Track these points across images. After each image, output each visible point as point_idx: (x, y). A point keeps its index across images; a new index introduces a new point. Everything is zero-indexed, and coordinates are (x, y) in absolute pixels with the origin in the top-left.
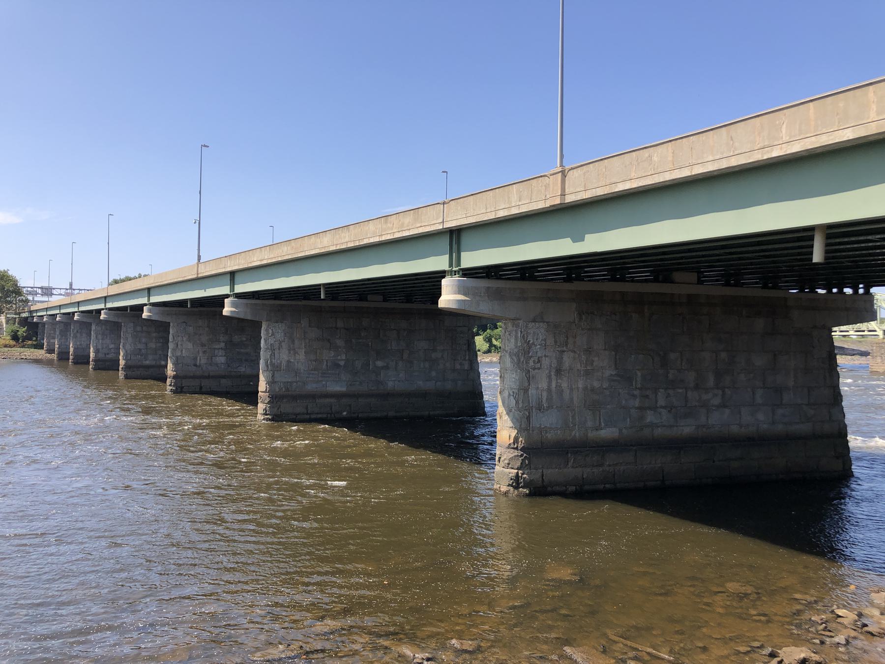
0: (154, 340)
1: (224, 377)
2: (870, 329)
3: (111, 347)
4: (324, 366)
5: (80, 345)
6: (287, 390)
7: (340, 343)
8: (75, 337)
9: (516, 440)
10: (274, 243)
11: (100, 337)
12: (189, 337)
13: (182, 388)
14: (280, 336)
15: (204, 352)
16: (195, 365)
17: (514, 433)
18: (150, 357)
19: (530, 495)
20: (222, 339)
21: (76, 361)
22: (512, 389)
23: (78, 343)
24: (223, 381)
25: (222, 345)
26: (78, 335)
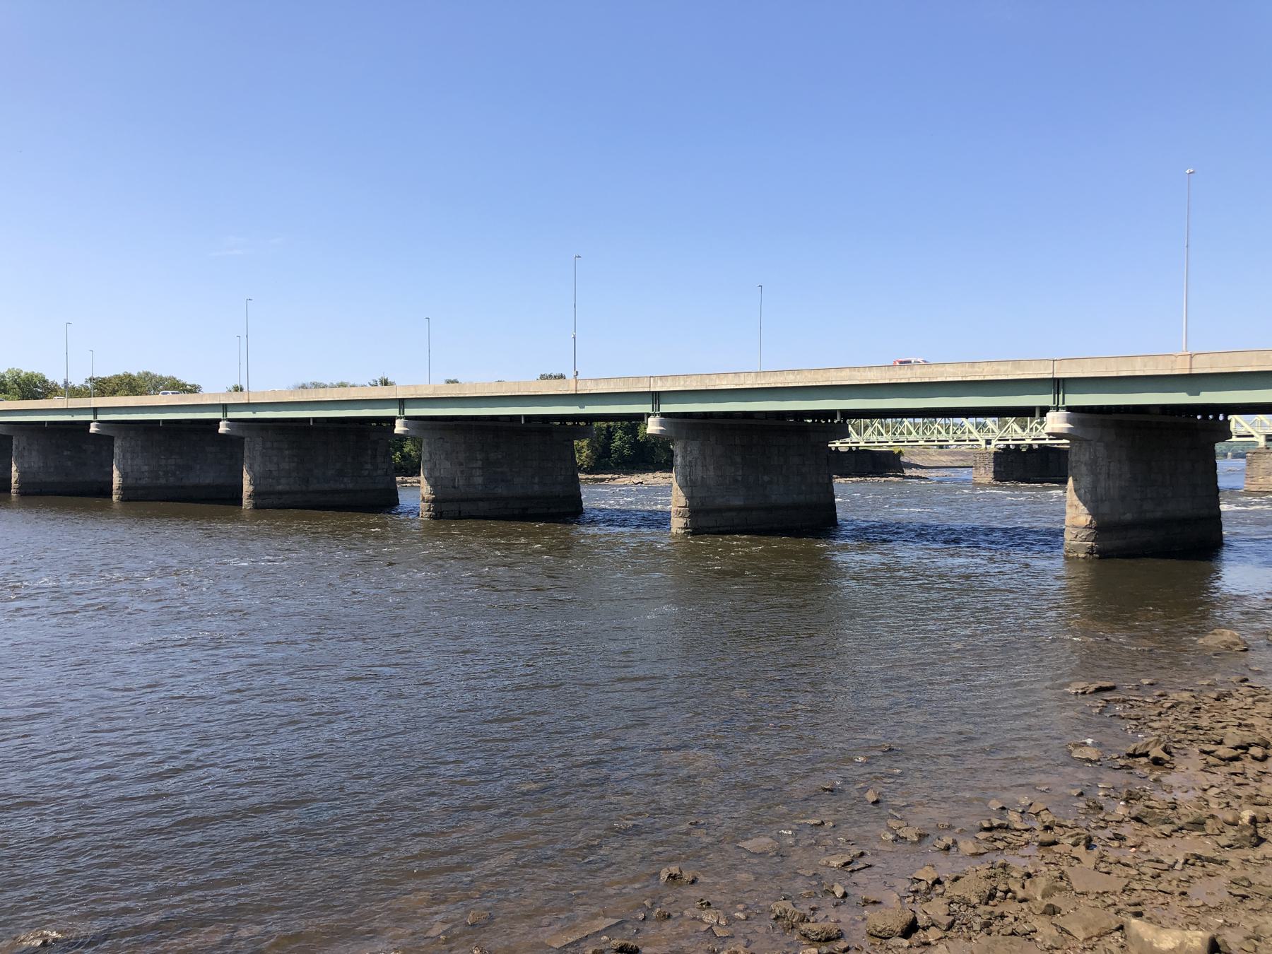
0: (287, 460)
1: (481, 500)
2: (971, 438)
3: (143, 470)
4: (728, 482)
5: (29, 468)
6: (703, 505)
7: (738, 459)
8: (20, 456)
9: (1091, 522)
10: (762, 370)
11: (128, 455)
12: (447, 454)
13: (441, 513)
14: (696, 453)
15: (462, 472)
16: (454, 487)
17: (1089, 518)
18: (283, 481)
19: (1099, 558)
20: (479, 457)
21: (22, 491)
22: (1087, 488)
23: (26, 466)
24: (481, 504)
25: (479, 463)
26: (26, 453)
